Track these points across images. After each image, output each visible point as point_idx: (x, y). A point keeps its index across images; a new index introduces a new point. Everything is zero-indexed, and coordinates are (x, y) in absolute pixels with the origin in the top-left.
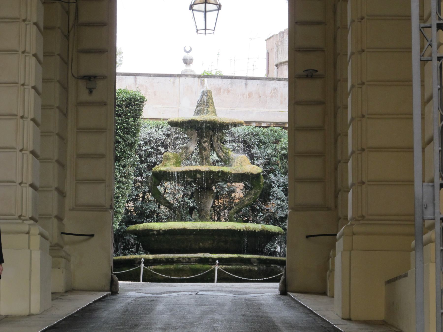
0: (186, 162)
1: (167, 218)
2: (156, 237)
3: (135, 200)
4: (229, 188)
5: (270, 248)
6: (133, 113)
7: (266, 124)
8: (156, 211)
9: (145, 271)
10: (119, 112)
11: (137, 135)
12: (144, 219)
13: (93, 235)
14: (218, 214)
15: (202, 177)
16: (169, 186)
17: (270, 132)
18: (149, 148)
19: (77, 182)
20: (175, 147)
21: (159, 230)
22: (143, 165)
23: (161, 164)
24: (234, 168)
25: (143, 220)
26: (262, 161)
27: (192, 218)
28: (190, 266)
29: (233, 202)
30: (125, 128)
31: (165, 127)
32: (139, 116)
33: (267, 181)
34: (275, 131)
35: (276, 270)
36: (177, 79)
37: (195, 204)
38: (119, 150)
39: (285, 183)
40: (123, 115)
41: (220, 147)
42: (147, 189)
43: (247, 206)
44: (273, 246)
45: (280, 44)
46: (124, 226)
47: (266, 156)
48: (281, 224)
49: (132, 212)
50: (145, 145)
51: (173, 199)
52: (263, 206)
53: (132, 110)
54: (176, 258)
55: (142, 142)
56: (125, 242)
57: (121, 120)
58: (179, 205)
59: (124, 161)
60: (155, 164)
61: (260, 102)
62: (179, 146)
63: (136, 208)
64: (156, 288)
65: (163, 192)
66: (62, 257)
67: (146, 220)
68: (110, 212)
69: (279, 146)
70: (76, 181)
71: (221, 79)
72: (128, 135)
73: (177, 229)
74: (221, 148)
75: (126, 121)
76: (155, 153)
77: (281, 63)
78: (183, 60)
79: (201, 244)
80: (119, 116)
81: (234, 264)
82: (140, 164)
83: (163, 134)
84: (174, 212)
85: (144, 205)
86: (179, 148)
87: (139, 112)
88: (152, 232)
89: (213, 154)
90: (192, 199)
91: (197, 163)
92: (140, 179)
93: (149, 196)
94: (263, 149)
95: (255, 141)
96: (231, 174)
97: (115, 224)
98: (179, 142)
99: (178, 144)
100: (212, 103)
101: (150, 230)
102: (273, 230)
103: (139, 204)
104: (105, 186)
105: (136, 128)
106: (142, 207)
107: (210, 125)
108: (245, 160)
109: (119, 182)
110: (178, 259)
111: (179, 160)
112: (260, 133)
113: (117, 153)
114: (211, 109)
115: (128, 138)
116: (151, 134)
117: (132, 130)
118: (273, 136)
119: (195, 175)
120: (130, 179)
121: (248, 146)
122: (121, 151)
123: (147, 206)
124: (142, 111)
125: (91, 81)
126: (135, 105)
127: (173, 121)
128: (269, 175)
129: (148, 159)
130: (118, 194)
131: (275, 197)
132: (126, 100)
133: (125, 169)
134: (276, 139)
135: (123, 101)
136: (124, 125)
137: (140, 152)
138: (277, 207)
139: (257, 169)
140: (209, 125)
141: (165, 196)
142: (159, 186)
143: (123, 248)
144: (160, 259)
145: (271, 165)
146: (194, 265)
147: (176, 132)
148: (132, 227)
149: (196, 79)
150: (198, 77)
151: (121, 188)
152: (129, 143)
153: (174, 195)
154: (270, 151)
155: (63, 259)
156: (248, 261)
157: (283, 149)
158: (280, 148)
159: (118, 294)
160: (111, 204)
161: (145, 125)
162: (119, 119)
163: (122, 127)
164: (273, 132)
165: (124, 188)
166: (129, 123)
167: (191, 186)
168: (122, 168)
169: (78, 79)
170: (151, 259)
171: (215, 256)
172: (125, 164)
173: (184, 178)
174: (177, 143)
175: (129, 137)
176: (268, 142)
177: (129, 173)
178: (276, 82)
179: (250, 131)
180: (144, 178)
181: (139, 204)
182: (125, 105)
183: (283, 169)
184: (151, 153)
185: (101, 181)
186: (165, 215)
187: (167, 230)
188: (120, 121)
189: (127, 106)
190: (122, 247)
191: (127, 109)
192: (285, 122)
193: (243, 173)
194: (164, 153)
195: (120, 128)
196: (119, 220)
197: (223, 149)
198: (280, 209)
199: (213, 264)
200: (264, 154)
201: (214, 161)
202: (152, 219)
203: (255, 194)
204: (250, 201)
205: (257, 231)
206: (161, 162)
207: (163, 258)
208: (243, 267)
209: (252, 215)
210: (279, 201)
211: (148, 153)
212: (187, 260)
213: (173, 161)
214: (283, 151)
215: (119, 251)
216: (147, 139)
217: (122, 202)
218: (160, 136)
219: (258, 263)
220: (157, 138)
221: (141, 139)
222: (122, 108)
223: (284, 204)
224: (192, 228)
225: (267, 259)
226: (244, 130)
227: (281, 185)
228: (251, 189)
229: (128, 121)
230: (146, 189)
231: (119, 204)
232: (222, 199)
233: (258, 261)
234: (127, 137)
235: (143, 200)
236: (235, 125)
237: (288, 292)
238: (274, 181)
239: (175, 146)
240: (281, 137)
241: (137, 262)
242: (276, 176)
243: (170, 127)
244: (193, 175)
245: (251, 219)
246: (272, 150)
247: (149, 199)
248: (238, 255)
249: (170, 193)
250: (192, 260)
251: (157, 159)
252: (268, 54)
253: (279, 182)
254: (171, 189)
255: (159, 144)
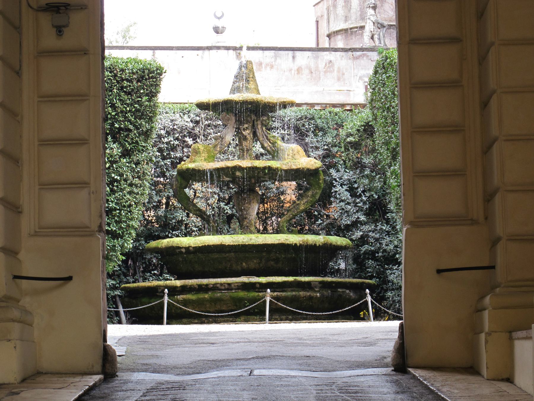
0: (221, 157)
1: (199, 230)
2: (185, 256)
3: (156, 208)
4: (278, 188)
5: (332, 265)
6: (147, 90)
7: (320, 106)
8: (184, 220)
9: (169, 303)
10: (128, 89)
11: (154, 120)
12: (169, 232)
13: (70, 278)
14: (264, 222)
15: (243, 175)
16: (200, 188)
17: (329, 115)
18: (172, 139)
19: (41, 187)
20: (207, 138)
21: (189, 247)
22: (166, 161)
23: (188, 160)
24: (285, 162)
25: (167, 234)
26: (320, 152)
27: (231, 229)
28: (231, 294)
29: (283, 206)
30: (137, 110)
31: (192, 112)
32: (155, 93)
33: (327, 178)
34: (335, 113)
35: (345, 295)
36: (207, 52)
37: (235, 211)
38: (129, 140)
39: (350, 180)
40: (134, 93)
41: (265, 135)
42: (171, 193)
43: (302, 212)
44: (336, 262)
45: (331, 8)
46: (143, 242)
47: (324, 145)
48: (346, 234)
49: (154, 223)
50: (167, 135)
51: (205, 204)
52: (322, 211)
53: (146, 86)
54: (212, 284)
55: (163, 132)
56: (145, 263)
57: (131, 100)
58: (213, 212)
59: (137, 155)
60: (181, 160)
61: (311, 79)
62: (211, 135)
63: (158, 218)
64: (183, 349)
65: (193, 196)
66: (13, 321)
67: (172, 234)
68: (99, 237)
69: (343, 132)
70: (39, 185)
71: (261, 51)
72: (142, 120)
73: (213, 245)
74: (267, 137)
75: (138, 101)
76: (181, 146)
77: (334, 32)
78: (213, 28)
79: (244, 264)
80: (128, 93)
81: (290, 289)
82: (161, 160)
83: (191, 120)
84: (208, 222)
85: (168, 214)
86: (211, 139)
87: (156, 88)
88: (179, 250)
89: (255, 145)
90: (230, 204)
91: (236, 157)
92: (162, 179)
93: (174, 202)
94: (321, 136)
95: (310, 127)
96: (281, 170)
97: (127, 243)
98: (211, 130)
99: (210, 134)
100: (254, 77)
101: (176, 247)
102: (339, 243)
103: (161, 212)
104: (89, 194)
105: (152, 110)
106: (166, 216)
107: (251, 107)
108: (299, 151)
109: (131, 185)
110: (215, 286)
111: (212, 154)
112: (316, 116)
113: (126, 145)
114: (252, 86)
115: (142, 124)
116: (175, 121)
117: (147, 113)
118: (333, 120)
119: (234, 174)
120: (146, 181)
121: (302, 134)
122: (133, 143)
123: (171, 214)
124: (159, 86)
125: (60, 13)
126: (149, 79)
127: (203, 103)
128: (329, 170)
129: (172, 153)
130: (129, 202)
131: (337, 198)
132: (137, 72)
133: (138, 167)
134: (336, 124)
135: (133, 73)
136: (136, 106)
137: (160, 144)
138: (340, 211)
139: (315, 163)
140: (250, 106)
141: (195, 201)
142: (186, 188)
143: (142, 269)
144: (191, 285)
145: (331, 157)
146: (235, 293)
147: (207, 117)
148: (153, 244)
149: (231, 52)
150: (233, 50)
151: (134, 193)
152: (142, 130)
153: (207, 199)
154: (329, 140)
155: (16, 324)
156: (307, 286)
157: (349, 135)
158: (345, 134)
159: (117, 376)
160: (101, 223)
161: (167, 110)
162: (128, 98)
163: (133, 110)
164: (332, 114)
165: (138, 194)
166: (143, 103)
167: (229, 188)
168: (134, 166)
169: (38, 11)
170: (179, 286)
171: (263, 280)
172: (138, 160)
173: (219, 177)
174: (209, 131)
175: (143, 123)
176: (326, 128)
177: (144, 172)
178: (331, 53)
179: (303, 114)
180: (167, 179)
181: (161, 212)
182: (136, 79)
183: (349, 162)
184: (175, 145)
185: (83, 184)
186: (195, 226)
187: (199, 247)
188: (129, 100)
189: (138, 81)
190: (141, 269)
191: (139, 84)
192: (345, 103)
193: (297, 169)
194: (191, 145)
195: (130, 111)
196: (132, 236)
197: (269, 138)
198: (344, 214)
199: (261, 290)
200: (322, 143)
201: (257, 155)
202: (179, 231)
203: (313, 196)
204: (307, 205)
205: (318, 245)
206: (188, 157)
207: (195, 284)
208: (301, 293)
209: (308, 222)
210: (344, 204)
211: (171, 146)
212: (227, 286)
213: (205, 155)
214: (349, 138)
215: (138, 275)
216: (169, 127)
217: (137, 212)
218: (186, 124)
219: (320, 287)
220: (182, 126)
221: (162, 128)
222: (132, 83)
223: (349, 207)
224: (232, 244)
225: (332, 282)
226: (296, 113)
227: (345, 183)
228: (307, 189)
229: (141, 101)
230: (170, 193)
231: (131, 215)
232: (269, 204)
233: (320, 285)
234: (139, 123)
235: (166, 207)
236: (284, 105)
237: (410, 367)
238: (336, 178)
239: (206, 136)
240: (344, 121)
241: (160, 290)
242: (338, 171)
243: (199, 110)
244: (231, 173)
245: (307, 228)
246: (332, 137)
247: (174, 206)
248: (295, 278)
249: (202, 198)
250: (233, 286)
251: (183, 154)
252: (317, 22)
253: (342, 179)
254: (203, 192)
255: (186, 133)
